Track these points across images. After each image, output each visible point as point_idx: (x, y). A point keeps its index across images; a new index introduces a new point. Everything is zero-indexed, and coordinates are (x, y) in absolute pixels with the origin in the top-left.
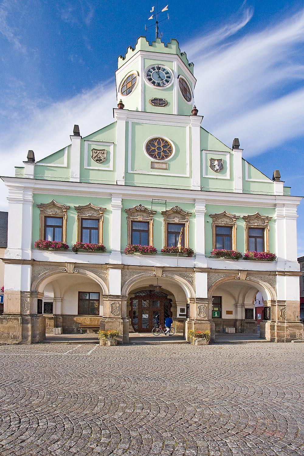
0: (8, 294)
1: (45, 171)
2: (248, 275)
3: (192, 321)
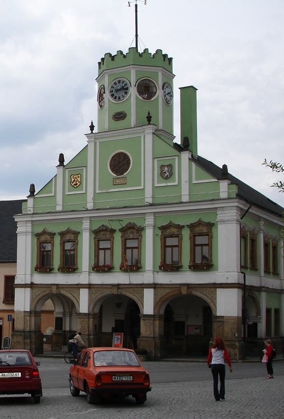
0: (17, 314)
2: (188, 288)
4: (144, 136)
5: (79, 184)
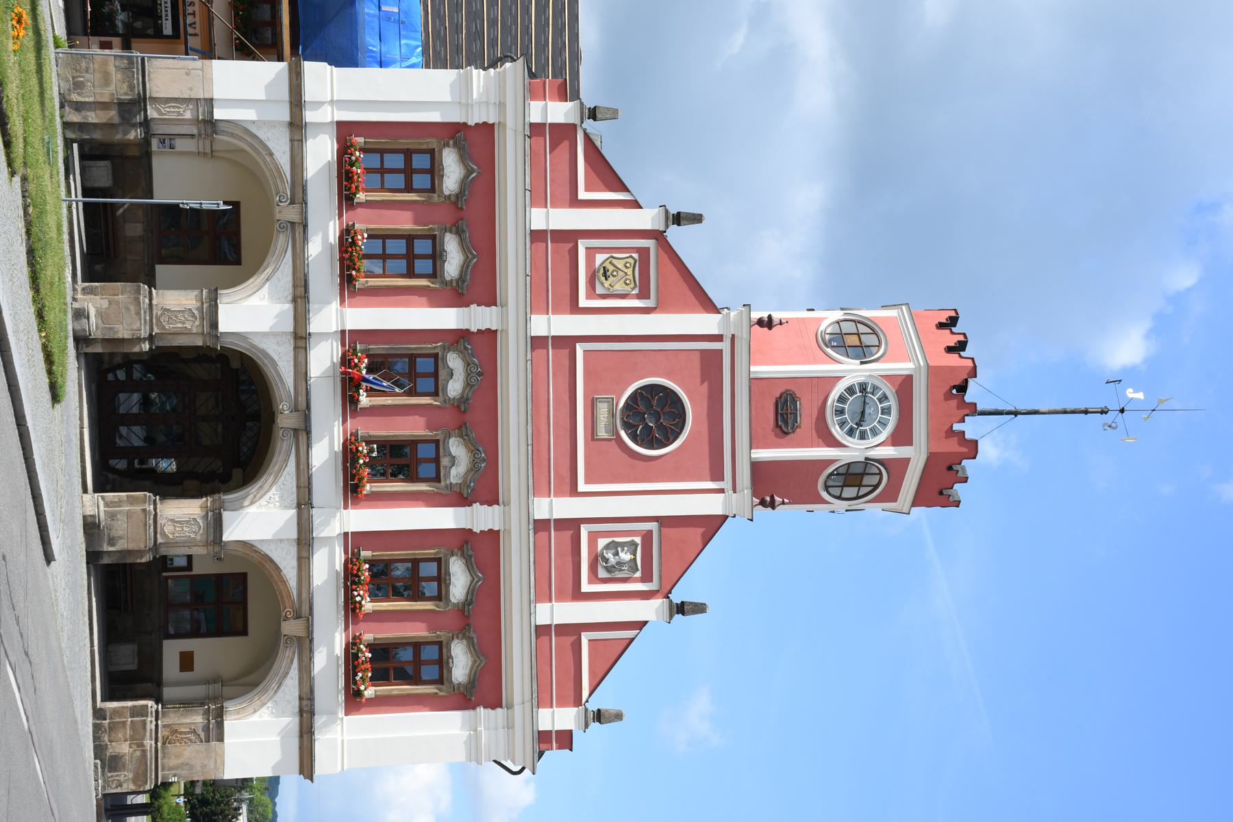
0: (202, 70)
2: (296, 431)
3: (152, 506)
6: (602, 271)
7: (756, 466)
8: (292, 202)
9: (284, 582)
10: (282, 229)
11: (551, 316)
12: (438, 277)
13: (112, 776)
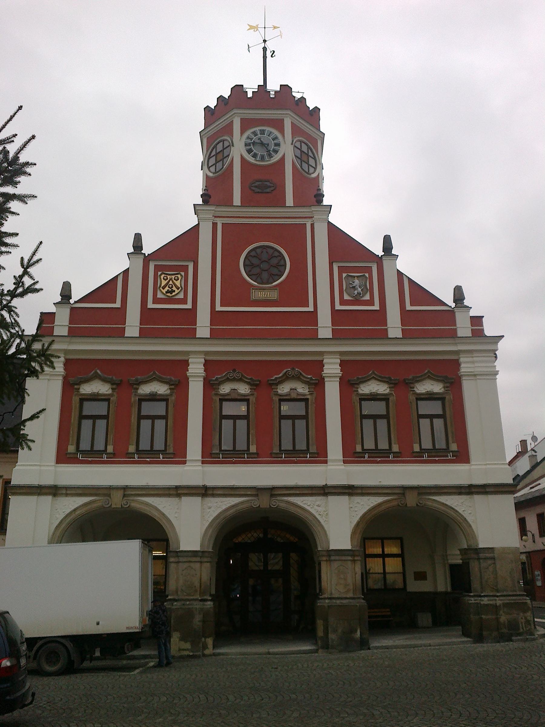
1: (2, 666)
2: (419, 494)
4: (312, 226)
5: (177, 291)
6: (169, 294)
7: (245, 202)
8: (109, 495)
9: (379, 505)
10: (127, 504)
11: (55, 324)
12: (444, 396)
13: (523, 628)
